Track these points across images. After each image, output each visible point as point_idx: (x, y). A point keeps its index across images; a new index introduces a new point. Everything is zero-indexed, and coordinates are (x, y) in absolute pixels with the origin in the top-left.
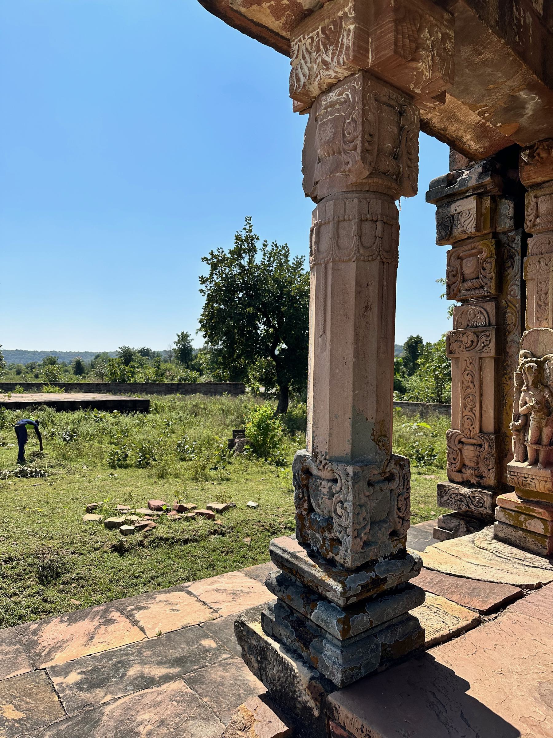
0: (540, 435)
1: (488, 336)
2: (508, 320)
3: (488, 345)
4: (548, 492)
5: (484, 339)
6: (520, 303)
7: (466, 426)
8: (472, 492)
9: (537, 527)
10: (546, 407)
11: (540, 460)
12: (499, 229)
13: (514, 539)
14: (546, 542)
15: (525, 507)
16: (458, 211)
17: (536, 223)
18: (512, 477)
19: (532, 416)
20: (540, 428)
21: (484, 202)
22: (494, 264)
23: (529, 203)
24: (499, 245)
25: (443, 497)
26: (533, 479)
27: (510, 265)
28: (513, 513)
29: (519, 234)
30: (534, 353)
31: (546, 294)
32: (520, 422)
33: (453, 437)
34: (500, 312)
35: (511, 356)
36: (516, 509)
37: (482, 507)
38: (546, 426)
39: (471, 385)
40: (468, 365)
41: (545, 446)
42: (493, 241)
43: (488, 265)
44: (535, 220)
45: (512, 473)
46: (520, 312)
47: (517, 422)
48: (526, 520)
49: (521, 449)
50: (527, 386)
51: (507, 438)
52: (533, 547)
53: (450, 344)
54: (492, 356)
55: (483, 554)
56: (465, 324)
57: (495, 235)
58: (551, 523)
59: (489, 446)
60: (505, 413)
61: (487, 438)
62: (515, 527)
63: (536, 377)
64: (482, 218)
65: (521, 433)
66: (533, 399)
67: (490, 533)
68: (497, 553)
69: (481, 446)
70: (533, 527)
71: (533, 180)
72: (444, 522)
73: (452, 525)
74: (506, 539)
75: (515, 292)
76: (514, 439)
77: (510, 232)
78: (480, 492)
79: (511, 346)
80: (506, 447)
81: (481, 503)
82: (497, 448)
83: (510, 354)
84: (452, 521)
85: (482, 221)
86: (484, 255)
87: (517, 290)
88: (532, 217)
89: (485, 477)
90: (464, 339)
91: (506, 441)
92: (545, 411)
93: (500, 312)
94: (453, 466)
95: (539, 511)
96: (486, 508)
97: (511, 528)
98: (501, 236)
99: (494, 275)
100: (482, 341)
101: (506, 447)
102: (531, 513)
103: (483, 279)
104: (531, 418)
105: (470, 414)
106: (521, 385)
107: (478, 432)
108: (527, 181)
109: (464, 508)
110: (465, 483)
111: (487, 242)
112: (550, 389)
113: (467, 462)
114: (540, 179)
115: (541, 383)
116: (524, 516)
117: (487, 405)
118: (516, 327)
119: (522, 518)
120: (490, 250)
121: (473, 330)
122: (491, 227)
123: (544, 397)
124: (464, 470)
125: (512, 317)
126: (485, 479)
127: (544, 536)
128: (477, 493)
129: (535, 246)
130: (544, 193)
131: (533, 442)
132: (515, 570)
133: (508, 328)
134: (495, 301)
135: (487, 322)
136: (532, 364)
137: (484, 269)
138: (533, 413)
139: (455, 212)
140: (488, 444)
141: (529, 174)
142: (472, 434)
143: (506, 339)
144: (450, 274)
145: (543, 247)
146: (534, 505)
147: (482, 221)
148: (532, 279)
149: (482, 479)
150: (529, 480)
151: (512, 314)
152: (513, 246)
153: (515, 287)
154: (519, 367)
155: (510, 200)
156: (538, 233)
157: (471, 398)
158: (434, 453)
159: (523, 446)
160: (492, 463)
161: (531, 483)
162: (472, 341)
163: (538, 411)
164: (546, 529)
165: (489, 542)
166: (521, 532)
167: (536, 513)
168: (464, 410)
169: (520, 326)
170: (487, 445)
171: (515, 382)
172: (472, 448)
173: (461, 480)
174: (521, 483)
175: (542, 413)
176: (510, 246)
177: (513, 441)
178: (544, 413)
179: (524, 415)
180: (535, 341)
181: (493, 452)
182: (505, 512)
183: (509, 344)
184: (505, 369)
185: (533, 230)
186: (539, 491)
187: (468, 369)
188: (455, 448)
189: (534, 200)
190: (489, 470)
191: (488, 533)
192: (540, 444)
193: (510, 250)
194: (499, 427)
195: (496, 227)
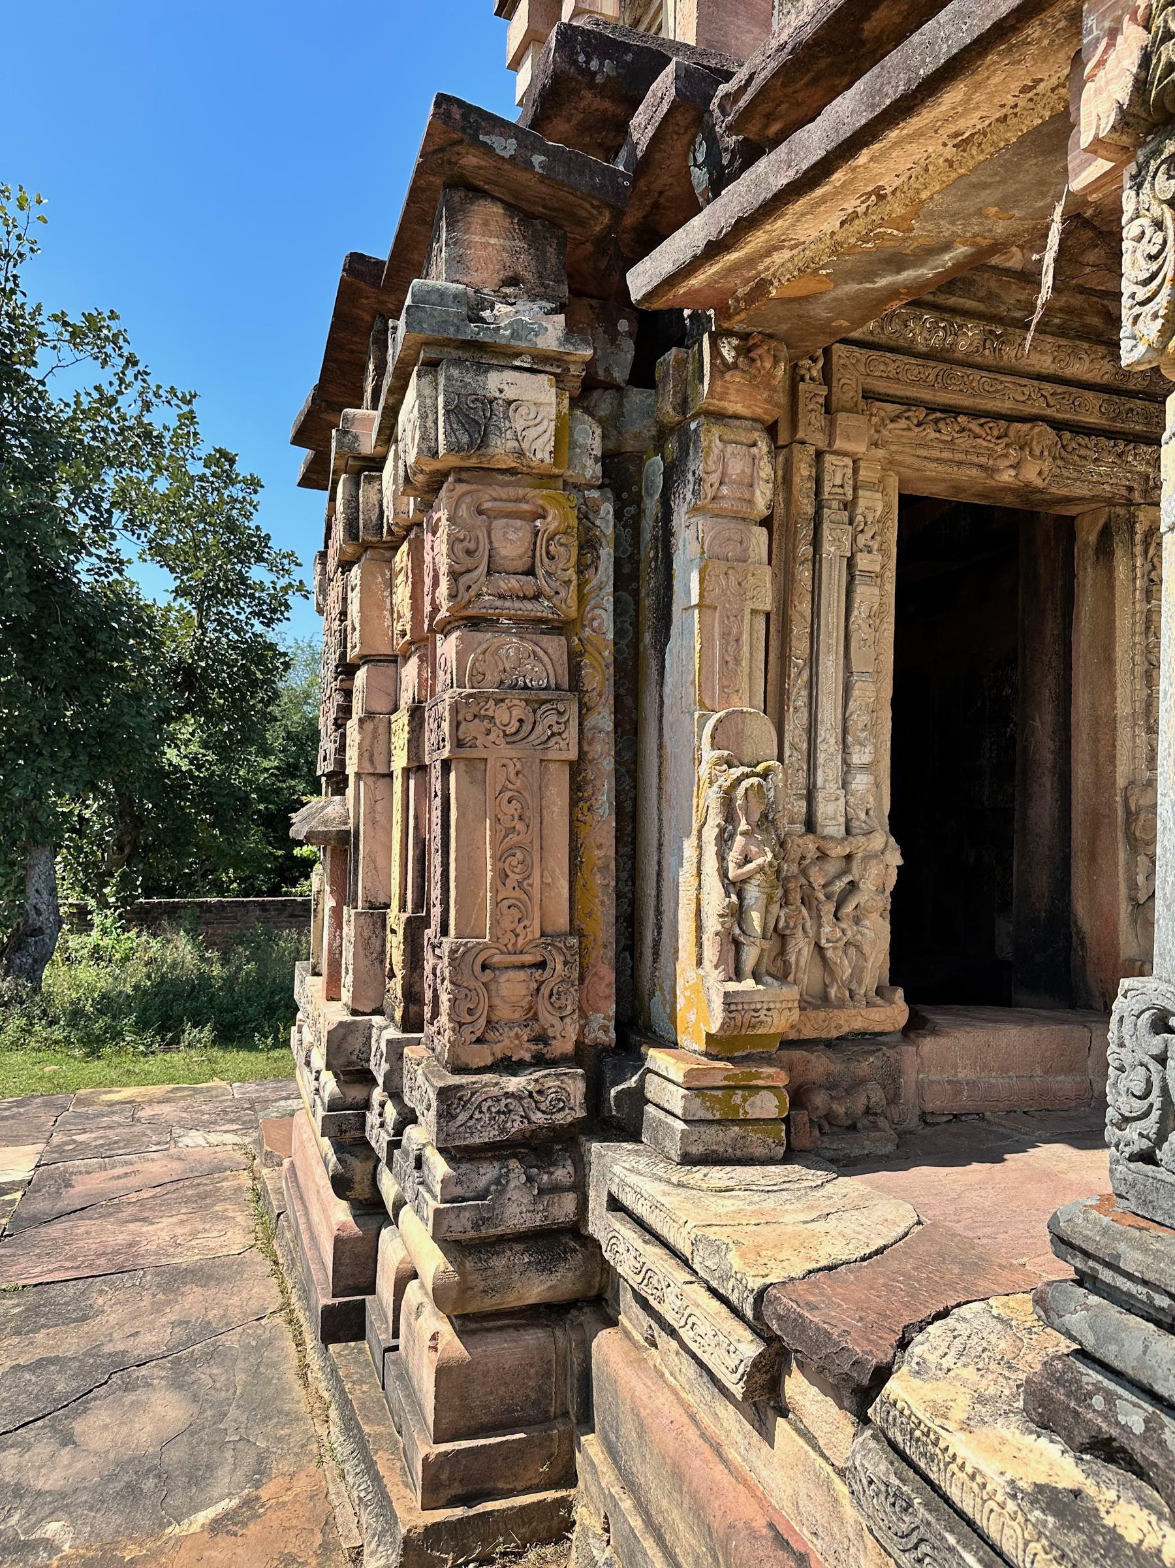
2: (586, 681)
5: (553, 718)
7: (507, 924)
8: (537, 1080)
16: (510, 394)
25: (453, 1117)
28: (719, 1093)
33: (469, 958)
37: (562, 1109)
39: (520, 826)
40: (512, 776)
45: (733, 1007)
48: (745, 1100)
52: (759, 1151)
53: (458, 724)
56: (492, 677)
59: (566, 963)
61: (561, 945)
69: (542, 965)
72: (459, 1182)
73: (482, 1182)
75: (601, 624)
78: (558, 1075)
81: (559, 1100)
84: (482, 1171)
86: (552, 522)
90: (501, 714)
94: (466, 1030)
97: (715, 1128)
100: (547, 722)
102: (755, 1082)
105: (518, 893)
107: (538, 935)
109: (516, 1126)
110: (509, 1066)
113: (504, 1012)
116: (740, 1092)
119: (737, 1098)
121: (525, 694)
124: (490, 1036)
126: (554, 1042)
128: (550, 1080)
139: (497, 395)
142: (519, 944)
144: (459, 547)
149: (546, 1044)
157: (519, 855)
162: (521, 721)
166: (736, 1129)
168: (500, 886)
170: (559, 960)
172: (522, 975)
173: (489, 1061)
182: (704, 1096)
187: (510, 786)
188: (472, 984)
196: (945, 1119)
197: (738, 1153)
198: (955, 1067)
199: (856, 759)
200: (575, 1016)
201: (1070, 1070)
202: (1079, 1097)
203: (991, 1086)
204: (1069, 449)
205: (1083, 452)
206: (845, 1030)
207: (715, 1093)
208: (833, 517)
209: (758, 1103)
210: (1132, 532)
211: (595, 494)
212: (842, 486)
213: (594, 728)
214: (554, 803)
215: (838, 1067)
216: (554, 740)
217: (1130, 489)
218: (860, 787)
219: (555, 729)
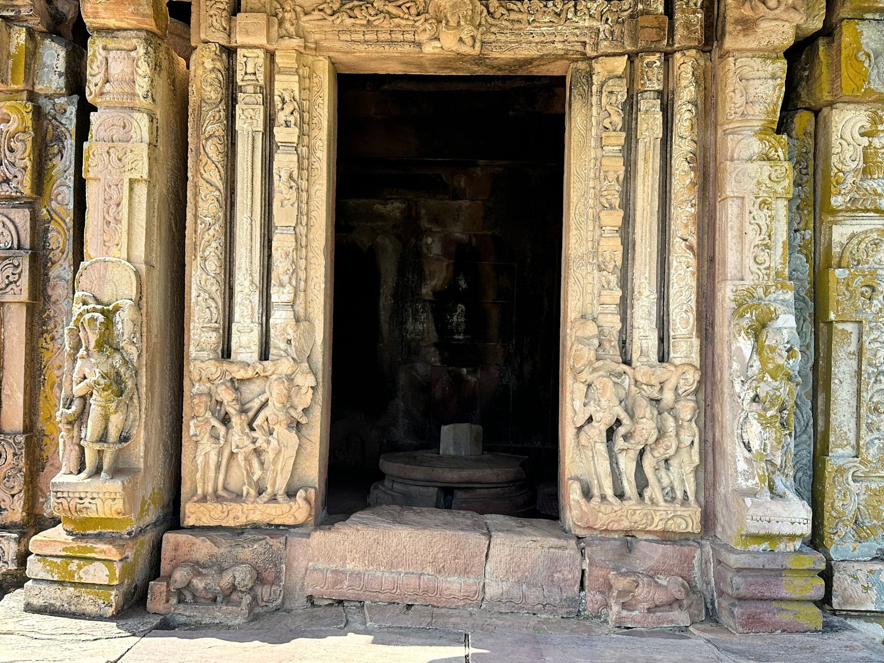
0: (106, 428)
1: (17, 267)
3: (16, 282)
4: (116, 516)
6: (72, 215)
9: (98, 574)
10: (116, 382)
11: (105, 467)
12: (38, 88)
13: (58, 604)
14: (111, 595)
15: (78, 547)
17: (105, 91)
18: (59, 501)
19: (94, 397)
20: (106, 415)
21: (14, 36)
22: (29, 145)
23: (94, 55)
24: (38, 113)
26: (93, 499)
27: (56, 151)
28: (59, 560)
29: (73, 103)
30: (99, 297)
31: (118, 205)
32: (74, 408)
34: (39, 230)
35: (54, 303)
36: (64, 553)
38: (116, 412)
41: (113, 443)
42: (30, 105)
43: (19, 144)
44: (103, 86)
45: (59, 495)
46: (71, 231)
47: (68, 408)
48: (80, 568)
49: (74, 452)
50: (87, 349)
51: (45, 439)
52: (90, 609)
54: (22, 300)
55: (8, 642)
57: (32, 96)
58: (120, 564)
59: (15, 454)
60: (42, 398)
61: (11, 441)
62: (61, 583)
63: (102, 335)
64: (10, 62)
65: (76, 426)
66: (97, 370)
67: (15, 604)
68: (33, 634)
70: (91, 577)
71: (102, 21)
74: (46, 607)
76: (62, 437)
77: (59, 98)
79: (55, 286)
80: (43, 453)
82: (27, 458)
83: (53, 299)
85: (10, 66)
87: (67, 195)
88: (99, 79)
89: (5, 509)
91: (44, 443)
92: (115, 388)
93: (39, 230)
95: (103, 549)
96: (6, 562)
97: (56, 586)
98: (42, 101)
99: (29, 164)
101: (43, 453)
102: (89, 555)
103: (9, 167)
104: (91, 401)
106: (77, 347)
108: (91, 20)
111: (19, 105)
112: (122, 355)
114: (112, 23)
115: (108, 344)
116: (76, 562)
117: (12, 386)
118: (65, 256)
119: (74, 565)
120: (23, 118)
122: (26, 80)
123: (113, 367)
125: (59, 239)
127: (109, 586)
129: (102, 127)
130: (118, 46)
131: (94, 439)
132: (67, 653)
133: (51, 256)
134: (29, 208)
135: (15, 243)
136: (96, 315)
137: (12, 151)
138: (95, 392)
140: (12, 451)
141: (96, 8)
143: (47, 275)
145: (114, 131)
146: (92, 540)
147: (10, 66)
148: (96, 179)
150: (87, 501)
151: (59, 232)
152: (63, 121)
153: (64, 188)
154: (74, 318)
155: (59, 44)
156: (108, 107)
158: (267, 374)
159: (77, 448)
160: (18, 483)
161: (90, 506)
163: (103, 390)
164: (111, 576)
165: (15, 619)
166: (72, 589)
167: (96, 553)
169: (71, 254)
170: (10, 452)
171: (67, 344)
174: (73, 509)
175: (110, 391)
176: (56, 120)
177: (61, 441)
178: (112, 392)
179: (81, 397)
180: (100, 278)
181: (22, 464)
183: (52, 283)
184: (44, 323)
185: (99, 100)
186: (103, 516)
189: (103, 53)
190: (13, 496)
191: (12, 604)
192: (105, 442)
193: (58, 127)
194: (31, 421)
195: (34, 84)
196: (326, 602)
197: (73, 608)
198: (344, 559)
199: (274, 298)
200: (21, 495)
201: (466, 572)
202: (466, 598)
203: (374, 578)
204: (497, 15)
205: (513, 16)
206: (242, 520)
207: (55, 560)
208: (247, 100)
209: (92, 572)
210: (590, 84)
211: (63, 100)
212: (255, 74)
213: (58, 277)
214: (14, 334)
215: (222, 550)
216: (10, 287)
217: (584, 44)
218: (278, 321)
219: (11, 279)
